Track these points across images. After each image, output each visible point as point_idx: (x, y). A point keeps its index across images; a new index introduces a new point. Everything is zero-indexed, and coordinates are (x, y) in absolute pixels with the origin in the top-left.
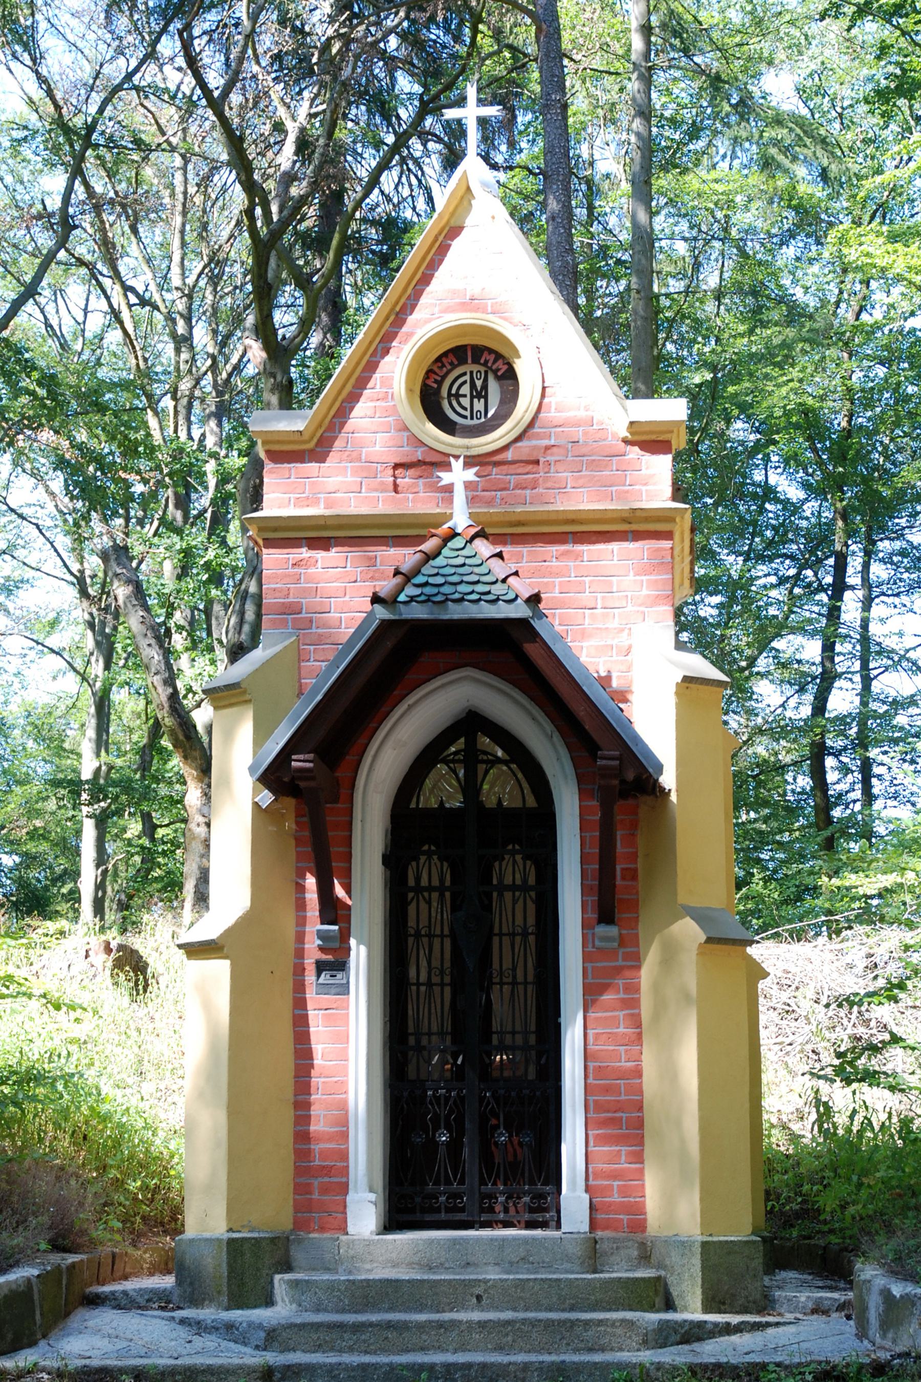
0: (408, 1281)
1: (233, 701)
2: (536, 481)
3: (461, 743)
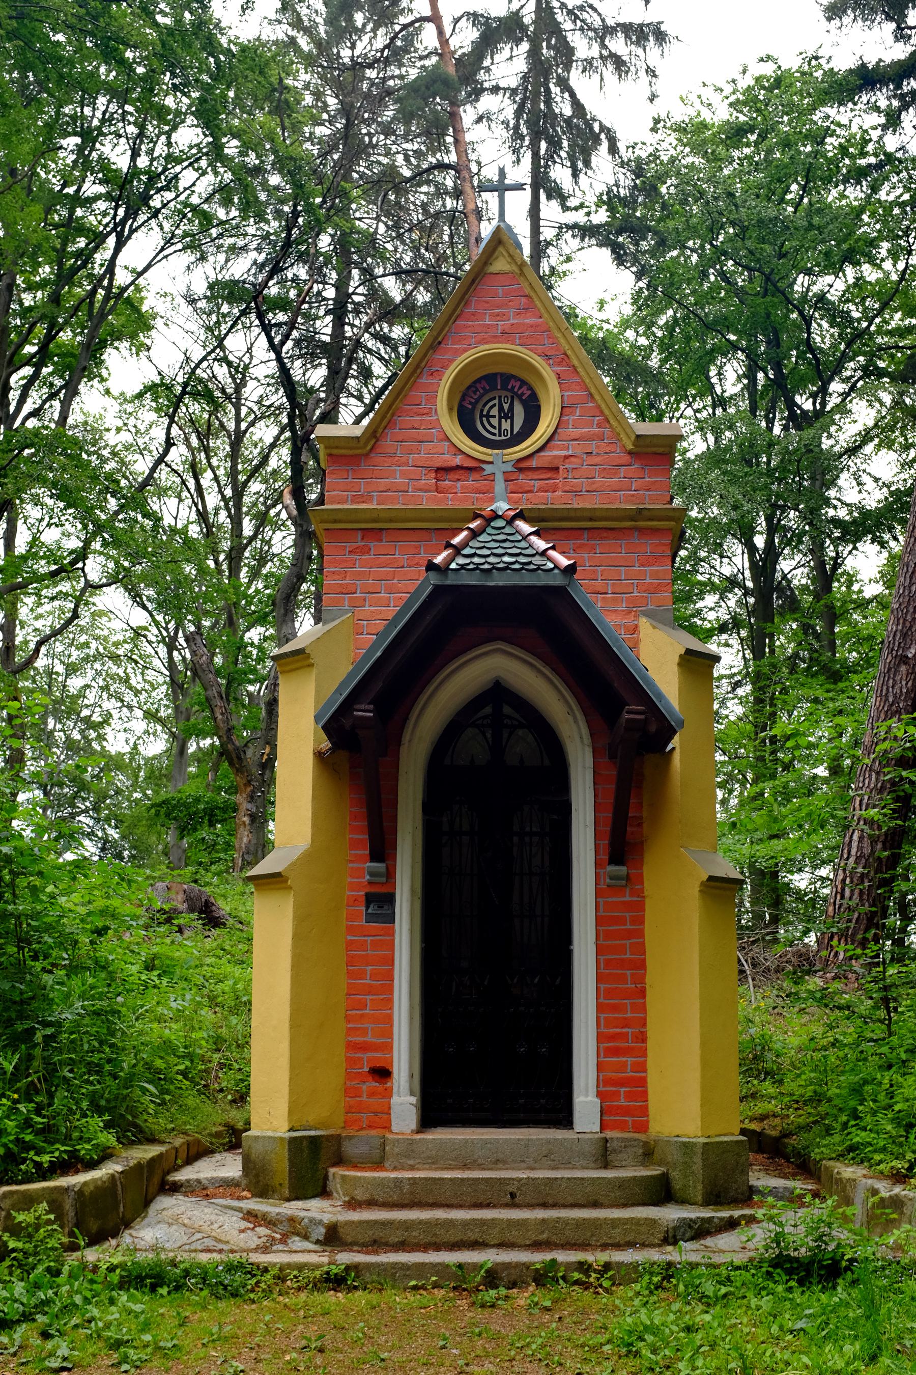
2: (556, 485)
3: (488, 710)
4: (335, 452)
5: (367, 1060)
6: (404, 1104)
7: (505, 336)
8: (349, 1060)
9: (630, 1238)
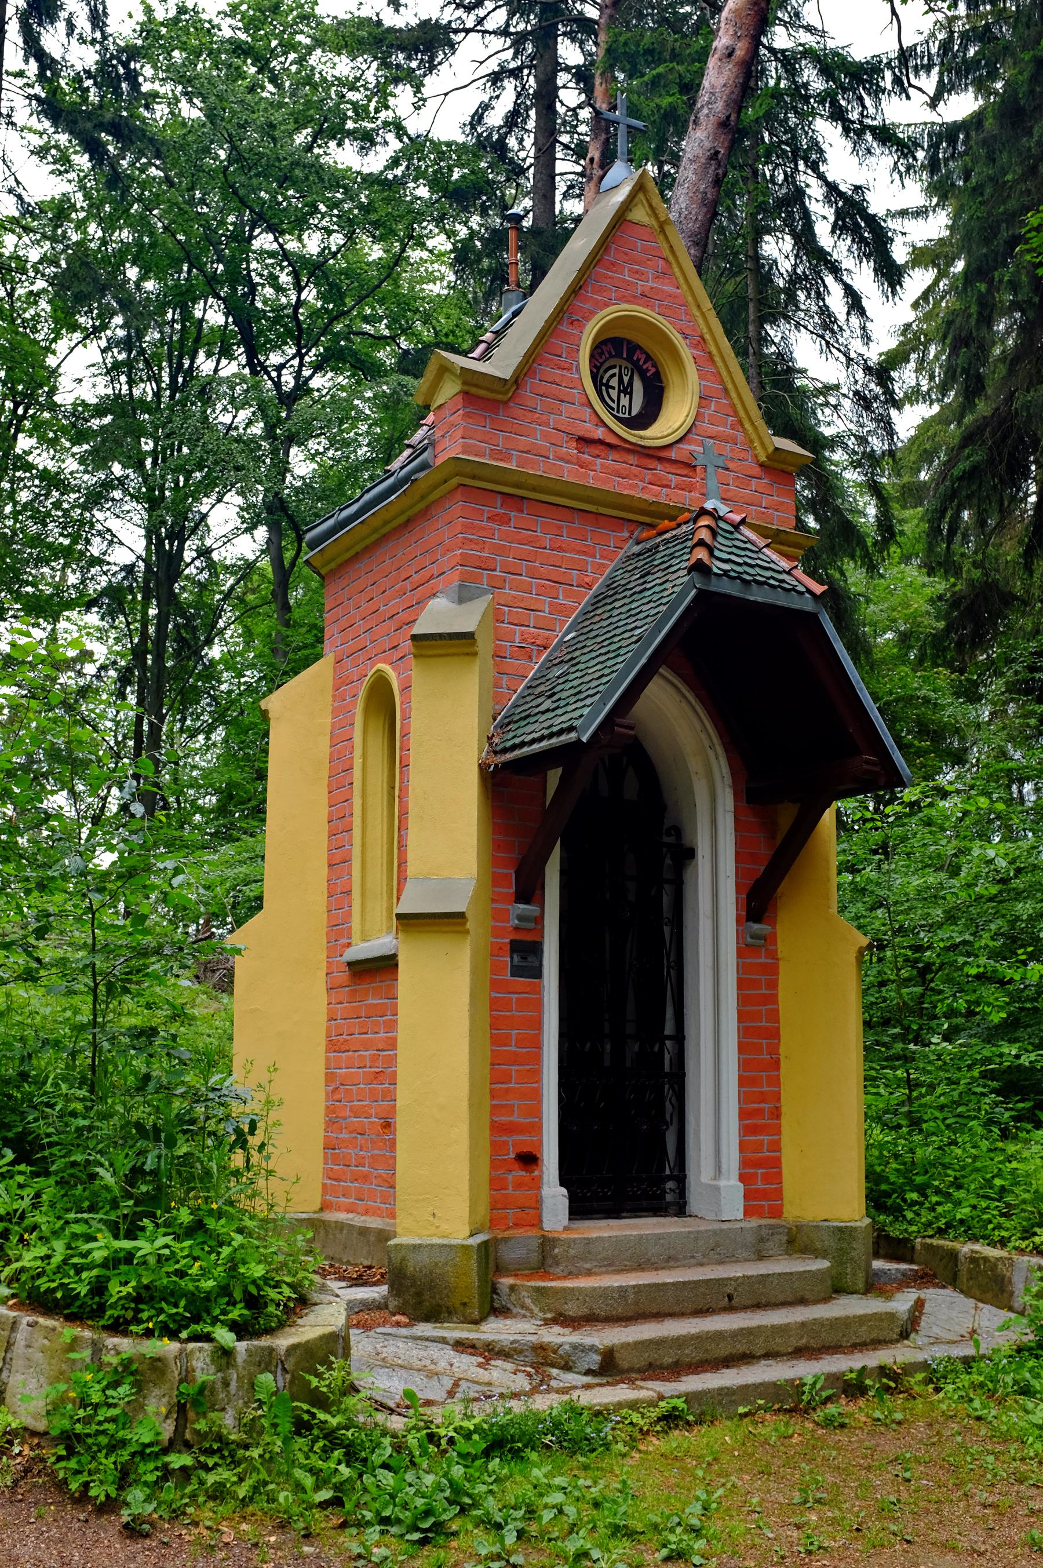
0: (673, 1284)
1: (450, 651)
2: (692, 484)
4: (473, 390)
5: (515, 1143)
6: (555, 1197)
7: (645, 299)
8: (493, 1144)
9: (874, 1335)
